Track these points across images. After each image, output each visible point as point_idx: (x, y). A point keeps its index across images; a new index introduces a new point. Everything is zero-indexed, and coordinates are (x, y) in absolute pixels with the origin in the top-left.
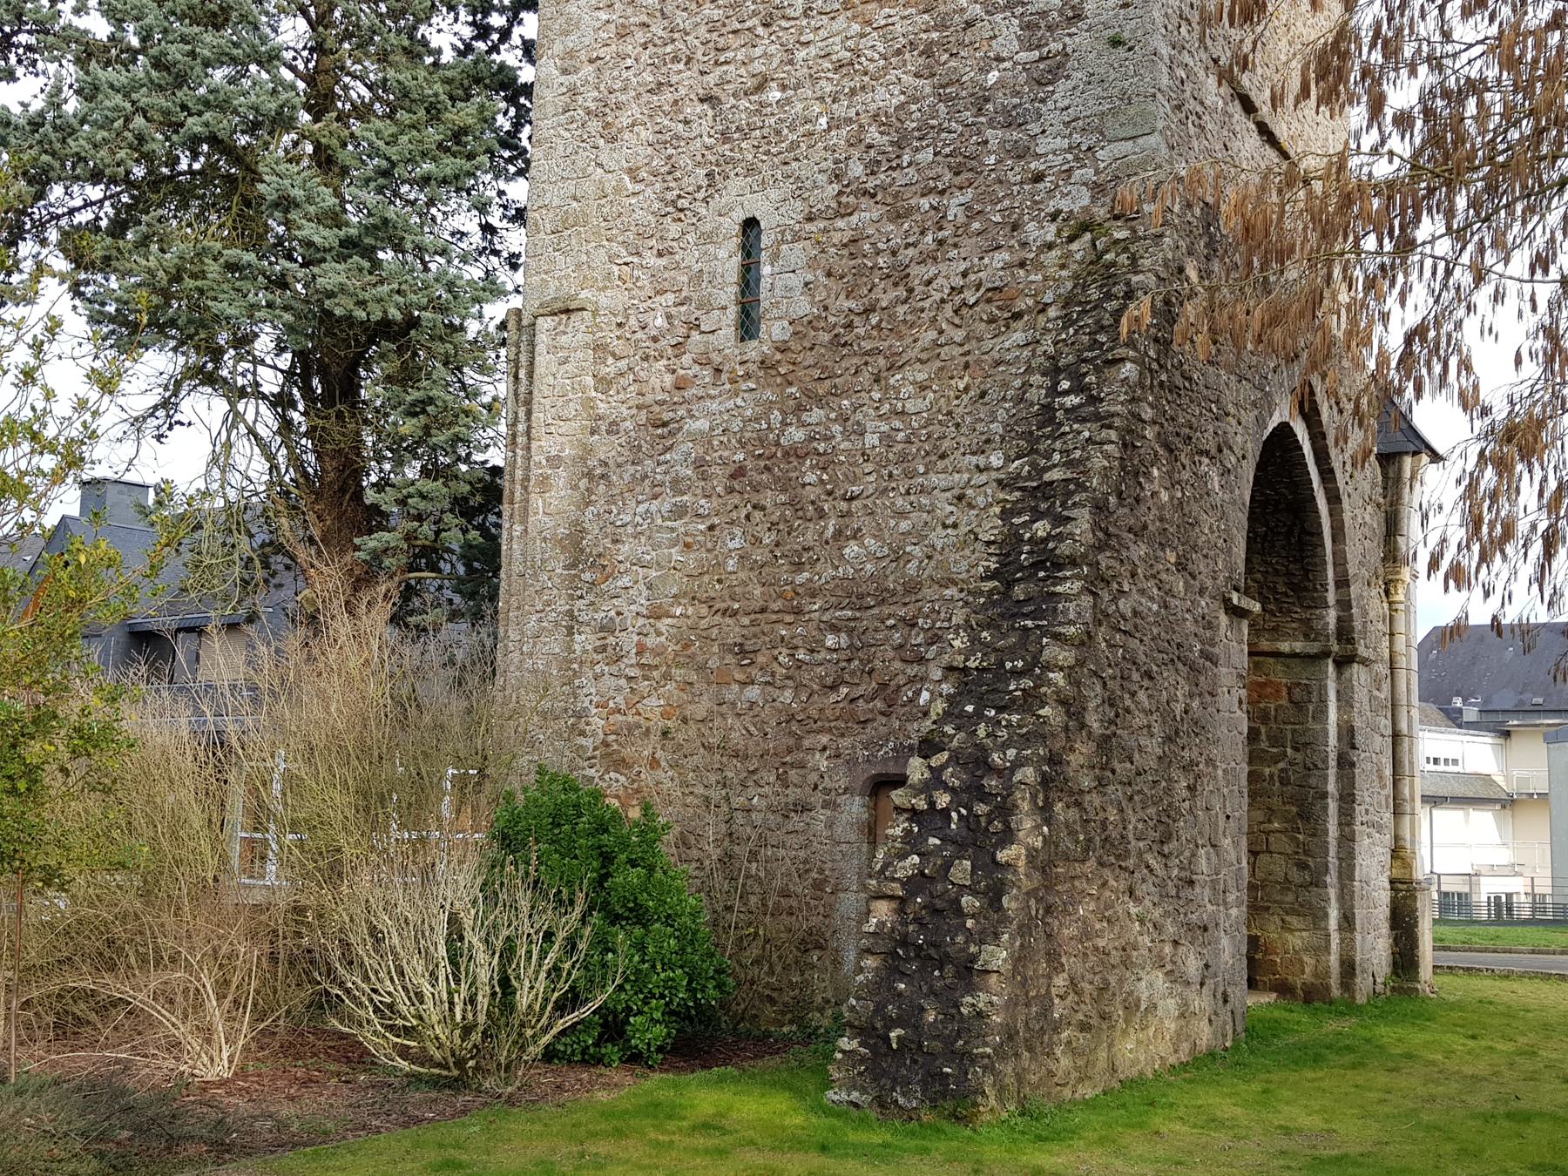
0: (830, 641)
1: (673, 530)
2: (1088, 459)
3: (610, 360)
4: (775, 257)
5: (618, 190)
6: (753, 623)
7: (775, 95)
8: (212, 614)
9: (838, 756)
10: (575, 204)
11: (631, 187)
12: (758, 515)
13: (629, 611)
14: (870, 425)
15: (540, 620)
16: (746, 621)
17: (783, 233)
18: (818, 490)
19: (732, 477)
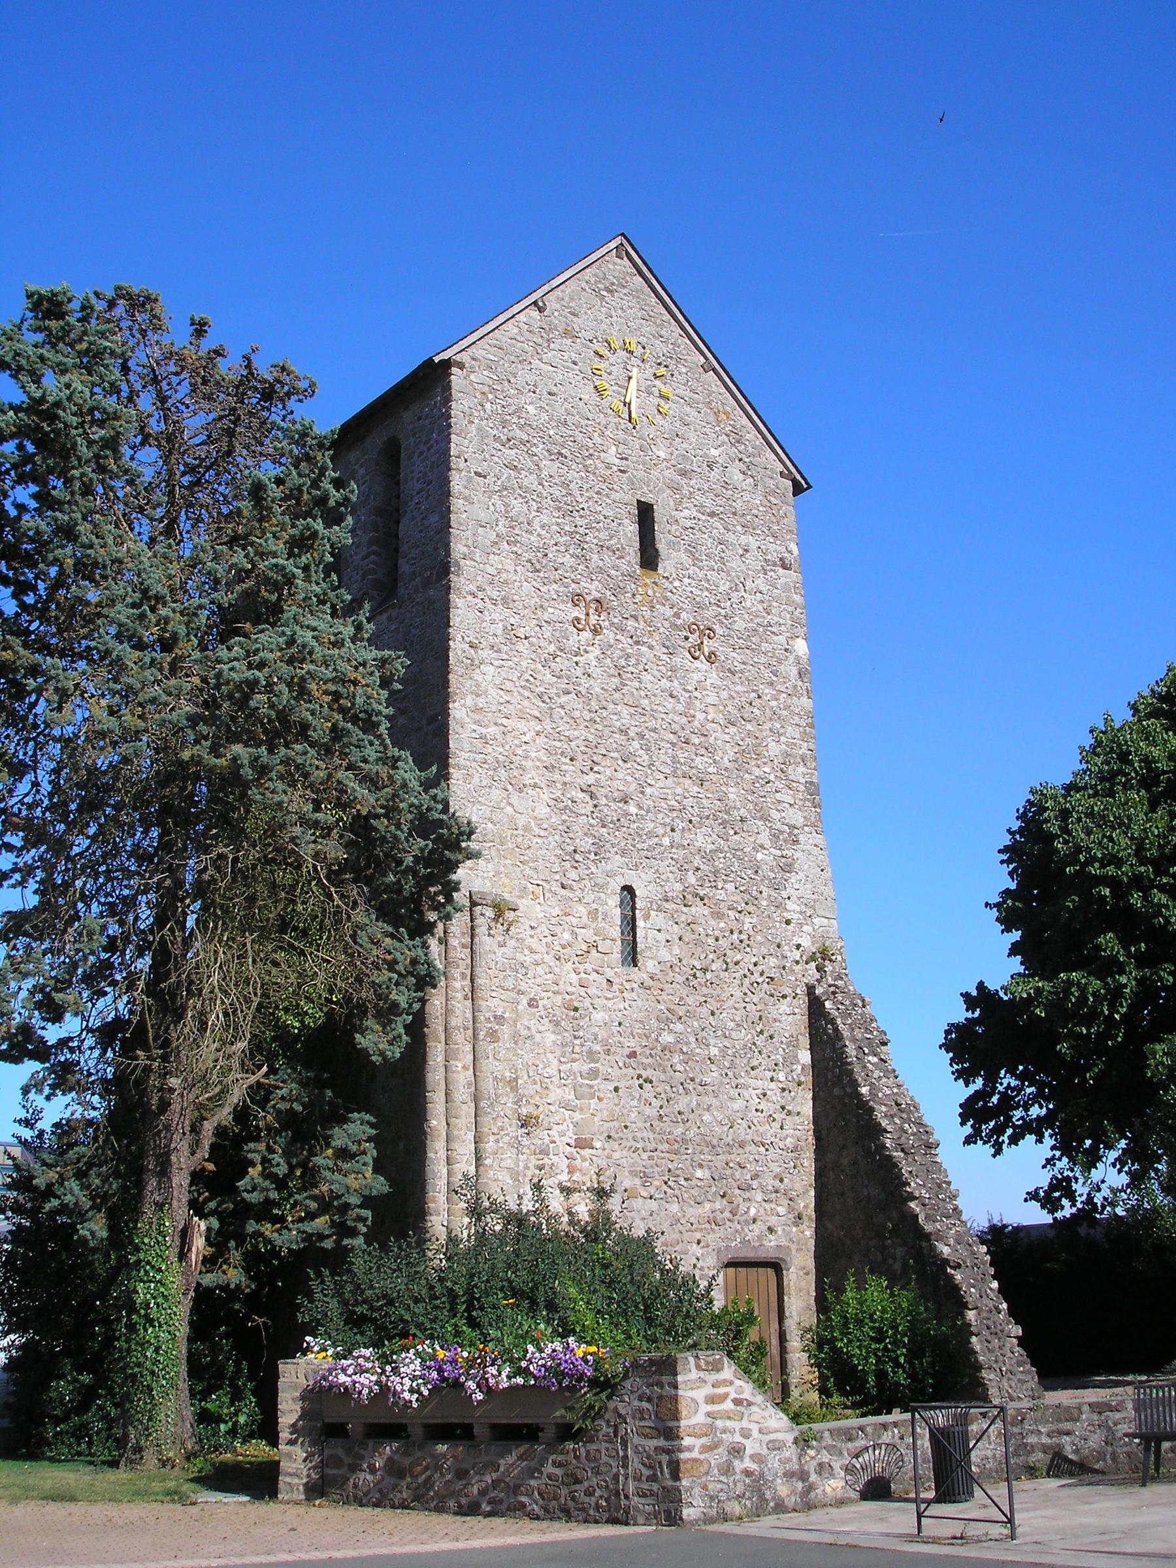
0: (699, 1173)
1: (591, 1087)
2: (49, 1445)
3: (526, 952)
4: (647, 917)
5: (527, 828)
6: (650, 1158)
7: (633, 809)
8: (1123, 980)
9: (708, 1246)
10: (490, 825)
11: (537, 831)
12: (647, 1086)
13: (561, 1142)
14: (712, 1041)
15: (497, 1141)
16: (645, 1156)
17: (651, 903)
18: (683, 1076)
19: (629, 1057)
